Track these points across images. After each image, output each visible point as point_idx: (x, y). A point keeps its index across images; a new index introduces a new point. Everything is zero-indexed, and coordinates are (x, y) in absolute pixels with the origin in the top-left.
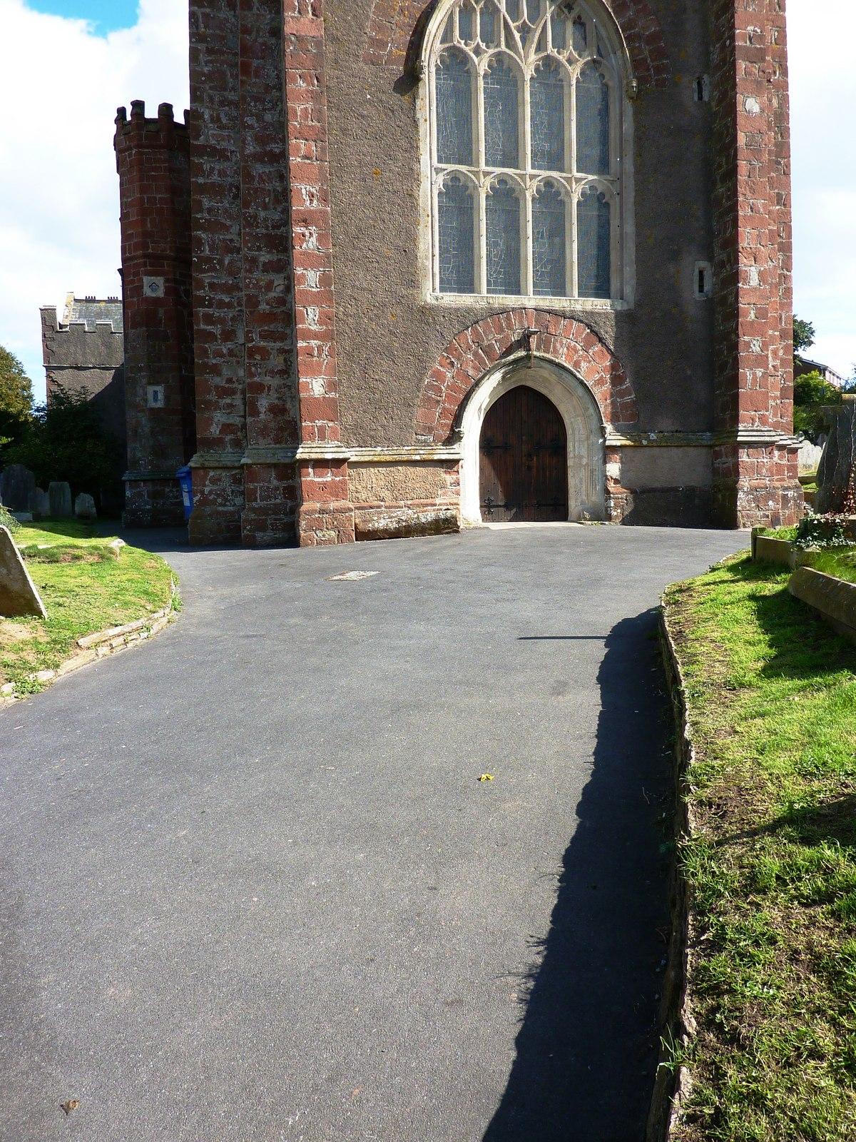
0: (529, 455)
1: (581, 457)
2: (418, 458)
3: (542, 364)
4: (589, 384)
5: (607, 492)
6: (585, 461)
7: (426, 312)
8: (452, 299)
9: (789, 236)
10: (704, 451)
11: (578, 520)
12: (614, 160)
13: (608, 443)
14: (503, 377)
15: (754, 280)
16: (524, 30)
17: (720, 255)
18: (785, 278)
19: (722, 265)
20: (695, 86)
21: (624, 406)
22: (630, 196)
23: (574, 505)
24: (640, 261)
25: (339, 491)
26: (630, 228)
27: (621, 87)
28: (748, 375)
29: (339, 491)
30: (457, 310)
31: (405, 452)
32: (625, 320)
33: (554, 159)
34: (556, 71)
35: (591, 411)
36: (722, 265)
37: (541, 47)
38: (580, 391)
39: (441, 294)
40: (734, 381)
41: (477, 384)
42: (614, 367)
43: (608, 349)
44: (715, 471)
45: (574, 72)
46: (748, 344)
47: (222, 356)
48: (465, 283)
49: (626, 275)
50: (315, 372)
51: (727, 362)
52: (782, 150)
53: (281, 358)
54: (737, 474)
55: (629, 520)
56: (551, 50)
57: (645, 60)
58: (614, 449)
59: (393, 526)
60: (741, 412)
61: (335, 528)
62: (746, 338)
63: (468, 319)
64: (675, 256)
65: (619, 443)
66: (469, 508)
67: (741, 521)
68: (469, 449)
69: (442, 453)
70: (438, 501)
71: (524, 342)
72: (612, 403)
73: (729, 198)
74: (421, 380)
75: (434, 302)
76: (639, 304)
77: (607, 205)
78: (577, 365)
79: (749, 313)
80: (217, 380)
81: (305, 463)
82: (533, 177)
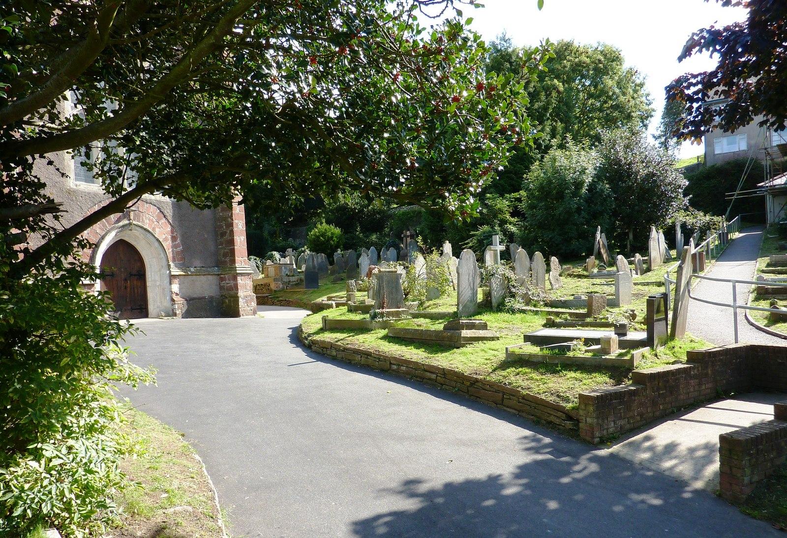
0: (126, 280)
1: (155, 281)
3: (137, 228)
5: (173, 300)
10: (215, 277)
11: (158, 317)
13: (172, 273)
21: (177, 253)
23: (152, 308)
30: (89, 193)
35: (162, 255)
38: (157, 244)
42: (172, 232)
43: (169, 222)
44: (221, 288)
46: (237, 224)
51: (226, 232)
54: (237, 289)
55: (188, 315)
58: (175, 276)
60: (236, 258)
67: (241, 312)
72: (173, 251)
75: (75, 187)
78: (154, 229)
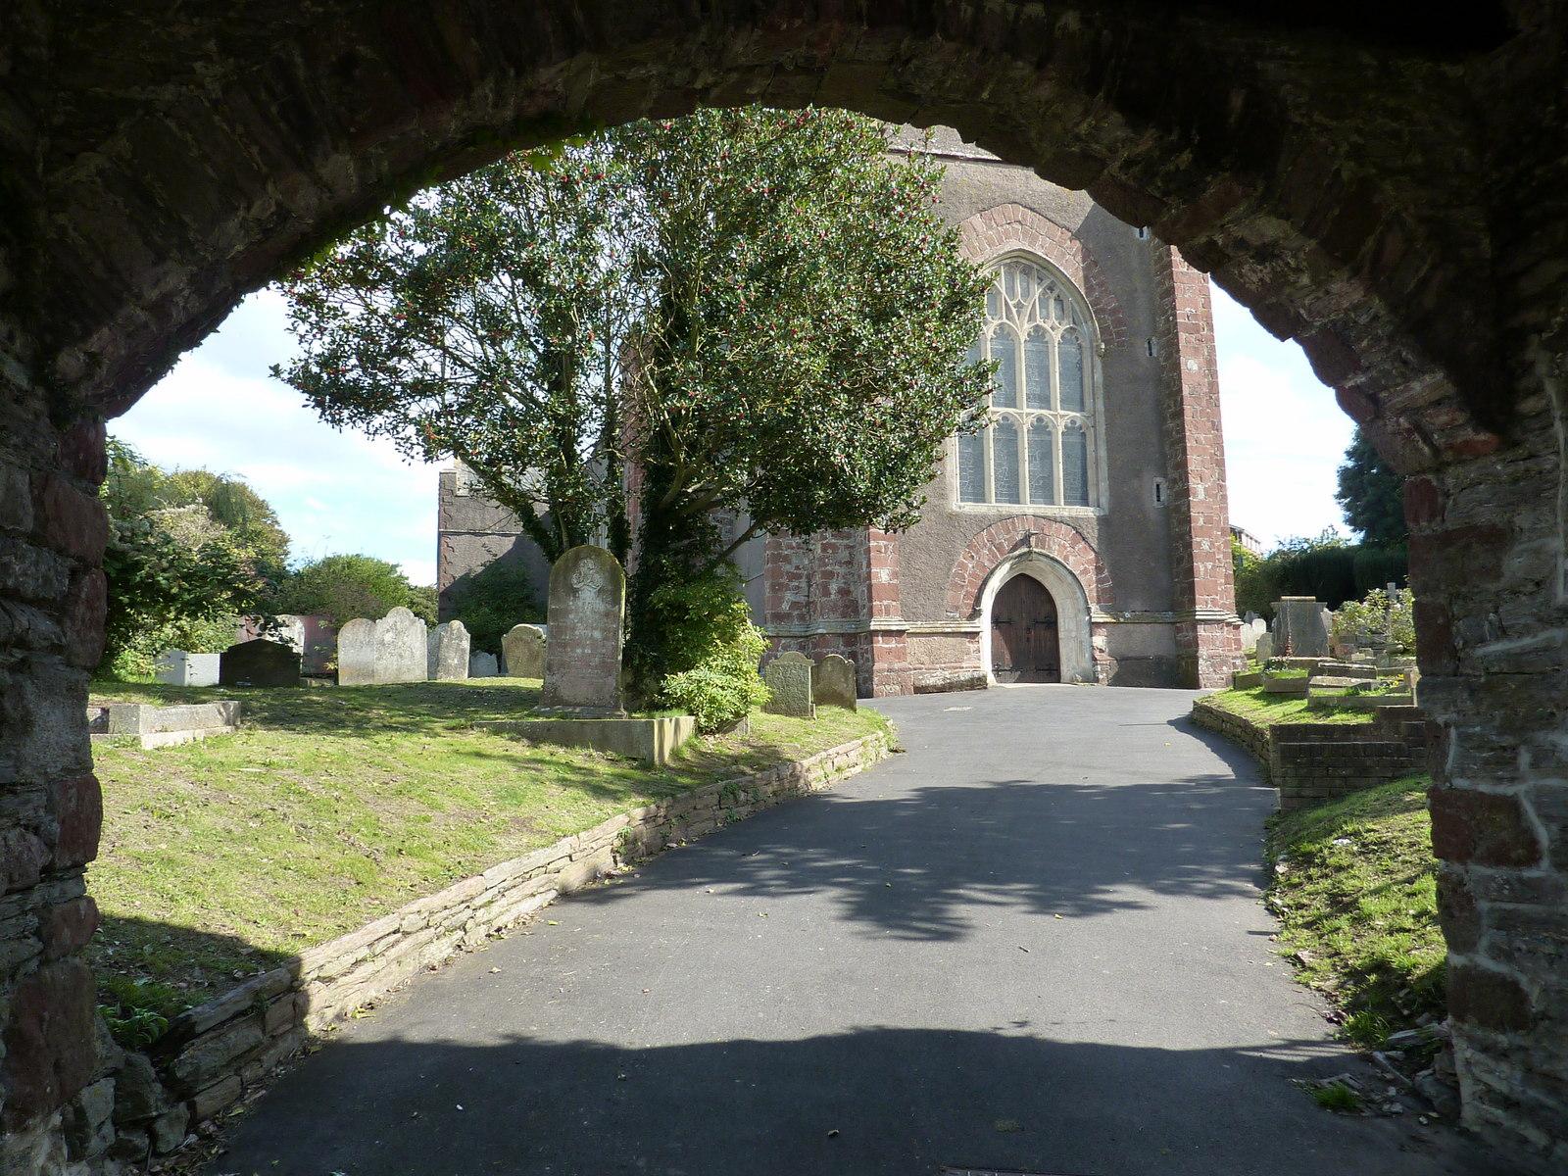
2: (949, 630)
3: (1041, 558)
4: (1076, 573)
5: (1094, 659)
6: (1074, 634)
7: (953, 518)
8: (970, 508)
9: (1223, 454)
10: (1167, 626)
11: (1072, 681)
12: (1088, 401)
13: (1093, 620)
14: (1011, 568)
15: (1201, 495)
16: (1019, 306)
17: (1173, 474)
18: (1222, 488)
19: (1175, 481)
20: (1146, 345)
21: (1104, 590)
22: (1102, 429)
23: (1065, 669)
24: (1112, 478)
25: (900, 655)
26: (1103, 453)
27: (1092, 347)
28: (1201, 568)
29: (900, 655)
31: (939, 626)
32: (1104, 522)
33: (1044, 401)
34: (1043, 336)
35: (1079, 594)
36: (1175, 481)
37: (1031, 318)
38: (1070, 578)
39: (963, 504)
40: (1190, 572)
41: (992, 572)
44: (1178, 644)
45: (1056, 336)
47: (793, 548)
48: (979, 496)
49: (1101, 486)
50: (882, 565)
52: (1214, 387)
53: (846, 553)
56: (1039, 321)
57: (1108, 327)
58: (1098, 625)
59: (940, 683)
61: (898, 683)
62: (1198, 539)
63: (983, 523)
64: (1138, 474)
65: (1101, 620)
66: (986, 667)
67: (1202, 682)
68: (984, 624)
69: (967, 627)
70: (964, 665)
71: (1025, 541)
73: (1178, 432)
74: (949, 569)
76: (1112, 510)
77: (1083, 435)
78: (1066, 558)
79: (1198, 519)
80: (788, 567)
81: (876, 632)
82: (1028, 415)
